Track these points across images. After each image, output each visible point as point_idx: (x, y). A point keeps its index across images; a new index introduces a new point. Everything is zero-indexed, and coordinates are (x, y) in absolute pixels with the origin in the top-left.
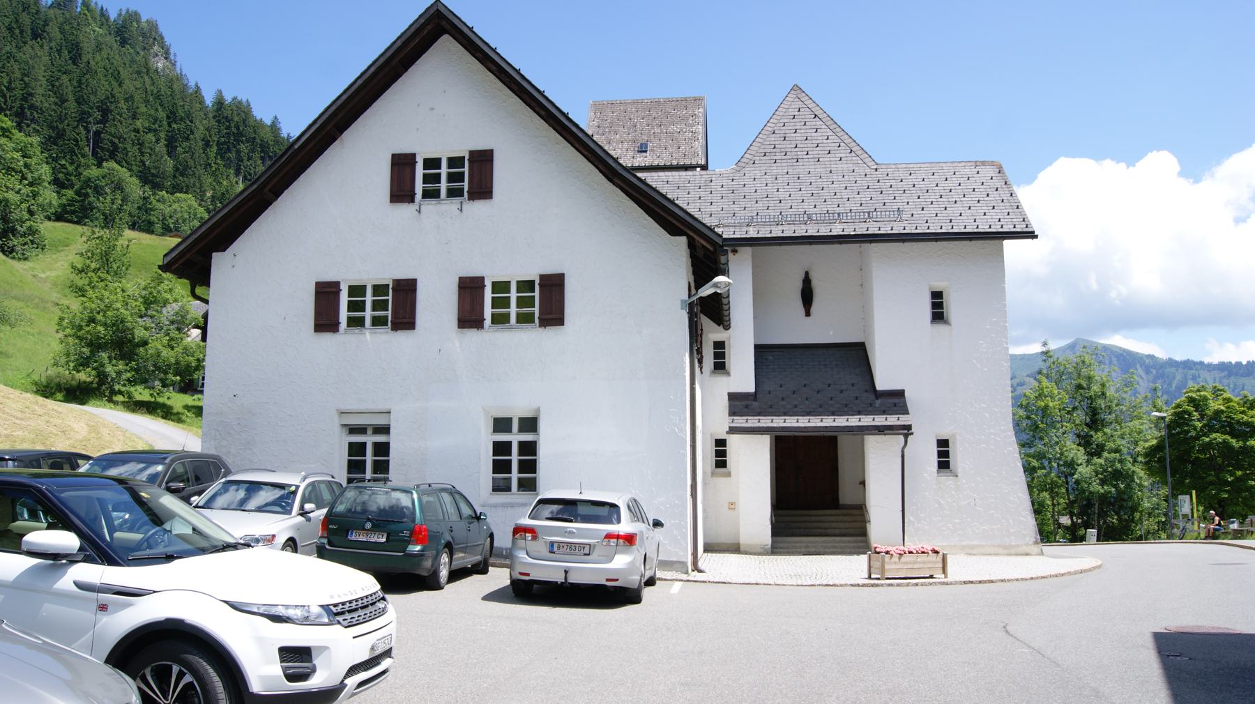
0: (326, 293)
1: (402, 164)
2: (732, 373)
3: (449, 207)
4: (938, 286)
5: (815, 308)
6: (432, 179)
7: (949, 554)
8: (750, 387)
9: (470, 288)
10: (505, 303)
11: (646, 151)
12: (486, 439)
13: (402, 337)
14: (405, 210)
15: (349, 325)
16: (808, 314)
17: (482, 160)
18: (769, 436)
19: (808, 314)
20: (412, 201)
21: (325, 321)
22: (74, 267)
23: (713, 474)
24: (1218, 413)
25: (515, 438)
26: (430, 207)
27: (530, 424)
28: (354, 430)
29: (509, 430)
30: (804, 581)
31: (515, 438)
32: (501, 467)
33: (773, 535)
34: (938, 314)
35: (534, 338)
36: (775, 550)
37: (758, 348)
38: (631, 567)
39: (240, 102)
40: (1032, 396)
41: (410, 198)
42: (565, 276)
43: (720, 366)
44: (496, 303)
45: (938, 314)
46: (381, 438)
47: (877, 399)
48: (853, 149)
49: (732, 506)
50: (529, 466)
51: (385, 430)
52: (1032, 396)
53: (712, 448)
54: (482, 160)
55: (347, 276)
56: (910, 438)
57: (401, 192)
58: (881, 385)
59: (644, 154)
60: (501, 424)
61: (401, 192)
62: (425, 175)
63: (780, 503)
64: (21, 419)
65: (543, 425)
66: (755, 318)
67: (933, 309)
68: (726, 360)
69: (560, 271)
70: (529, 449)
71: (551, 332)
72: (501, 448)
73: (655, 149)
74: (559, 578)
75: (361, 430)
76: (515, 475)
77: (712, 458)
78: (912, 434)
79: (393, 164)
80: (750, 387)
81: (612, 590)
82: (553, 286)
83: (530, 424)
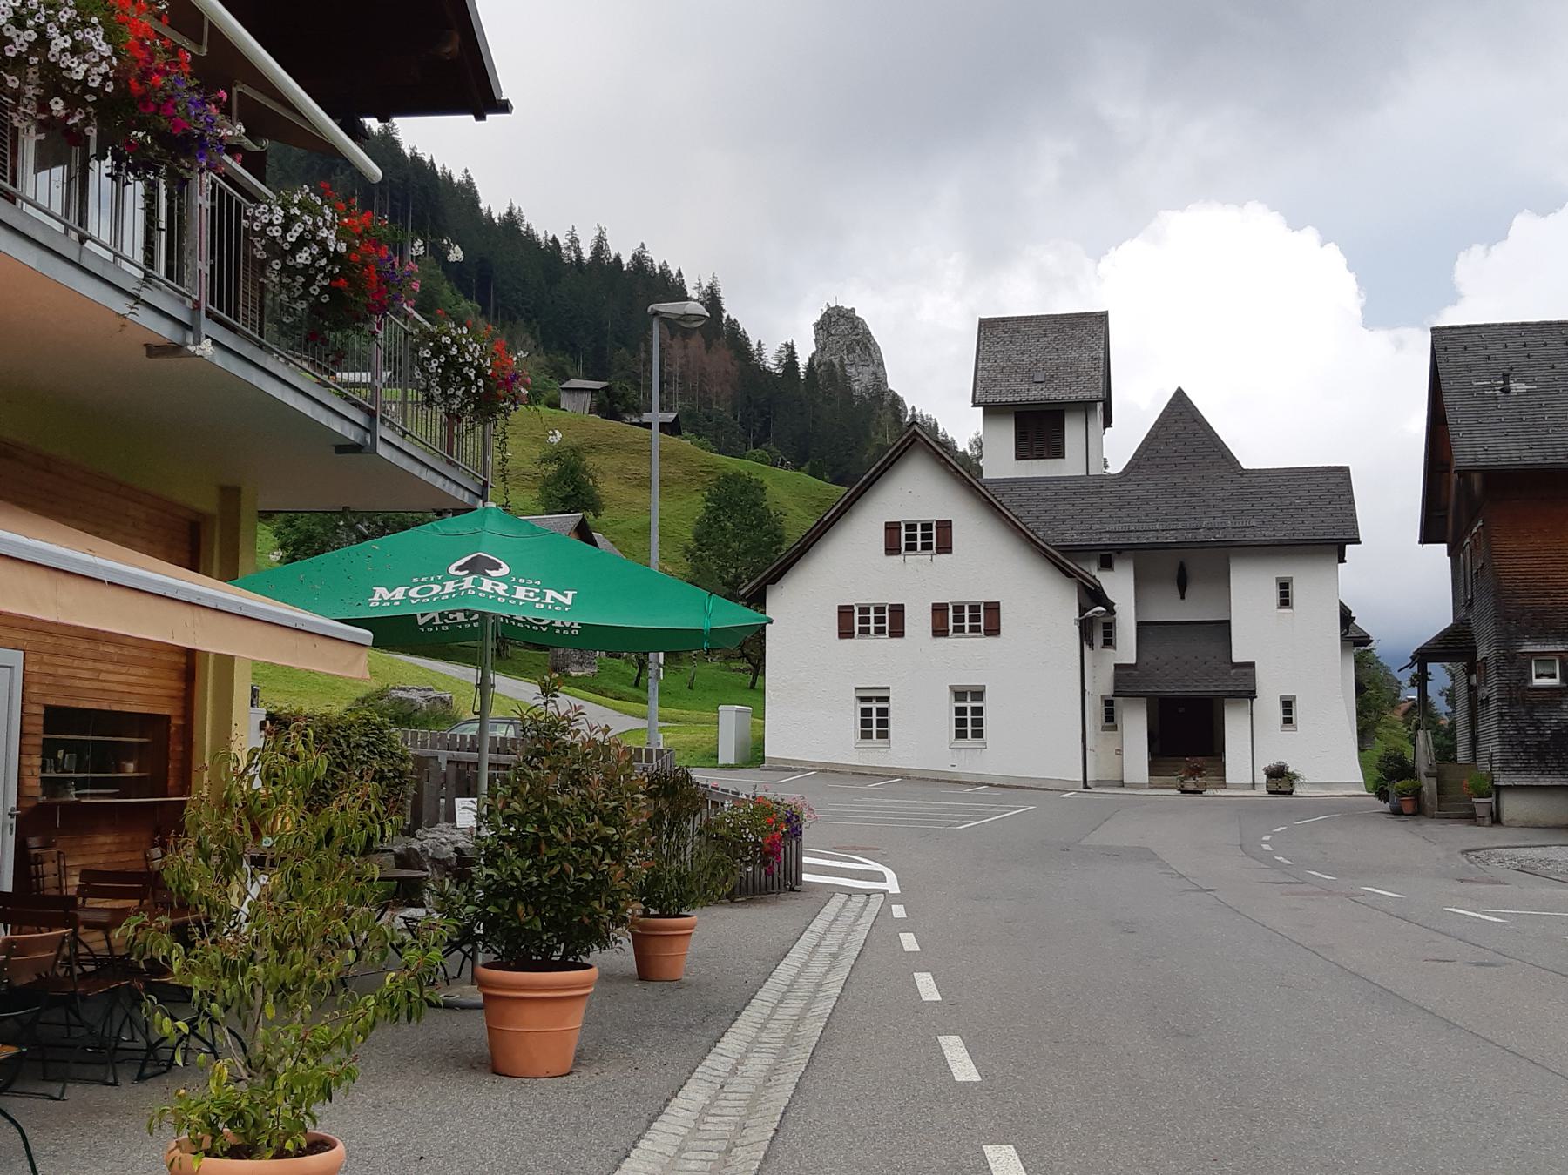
0: (845, 612)
1: (892, 529)
3: (925, 557)
7: (625, 978)
15: (860, 633)
16: (1183, 597)
17: (945, 526)
19: (1183, 597)
20: (900, 553)
21: (845, 632)
25: (969, 704)
26: (912, 558)
27: (979, 694)
28: (863, 699)
33: (1150, 775)
34: (1285, 602)
37: (1138, 624)
39: (421, 161)
40: (747, 1122)
41: (898, 552)
43: (1109, 642)
44: (956, 619)
45: (1285, 602)
47: (1233, 669)
51: (886, 699)
52: (747, 1122)
53: (1101, 707)
56: (1255, 700)
57: (892, 549)
60: (959, 694)
61: (892, 549)
65: (987, 696)
66: (1136, 602)
67: (1281, 596)
75: (869, 699)
76: (969, 728)
77: (1101, 715)
78: (1256, 697)
79: (886, 529)
83: (979, 694)
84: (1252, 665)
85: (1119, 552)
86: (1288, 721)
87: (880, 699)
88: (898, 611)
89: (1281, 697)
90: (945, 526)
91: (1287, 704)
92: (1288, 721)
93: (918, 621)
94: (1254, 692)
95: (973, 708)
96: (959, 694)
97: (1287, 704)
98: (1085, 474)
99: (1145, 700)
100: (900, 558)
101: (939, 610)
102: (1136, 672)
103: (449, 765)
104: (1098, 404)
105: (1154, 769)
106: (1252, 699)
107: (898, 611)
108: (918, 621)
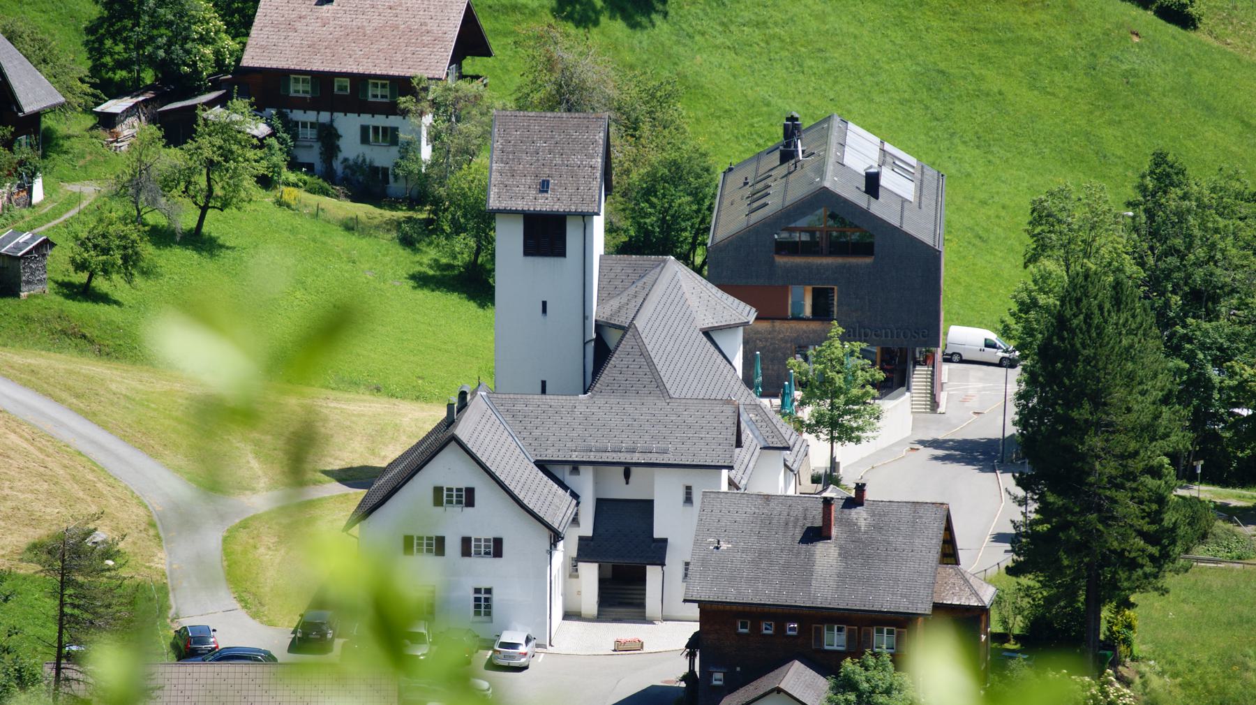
1: (438, 491)
2: (581, 523)
6: (450, 496)
8: (590, 533)
9: (466, 541)
11: (547, 192)
12: (472, 596)
14: (440, 509)
16: (627, 483)
17: (470, 492)
18: (596, 565)
19: (627, 483)
22: (73, 261)
24: (1027, 384)
25: (483, 596)
26: (450, 509)
27: (489, 591)
29: (480, 593)
30: (718, 361)
31: (483, 596)
32: (477, 606)
35: (491, 561)
36: (600, 617)
38: (526, 661)
42: (472, 306)
46: (487, 596)
49: (579, 593)
50: (488, 607)
54: (470, 492)
55: (416, 534)
58: (657, 535)
59: (546, 195)
60: (477, 591)
64: (77, 396)
70: (487, 600)
71: (497, 559)
72: (477, 600)
73: (556, 187)
74: (507, 664)
80: (590, 533)
82: (498, 542)
83: (489, 591)
95: (485, 598)
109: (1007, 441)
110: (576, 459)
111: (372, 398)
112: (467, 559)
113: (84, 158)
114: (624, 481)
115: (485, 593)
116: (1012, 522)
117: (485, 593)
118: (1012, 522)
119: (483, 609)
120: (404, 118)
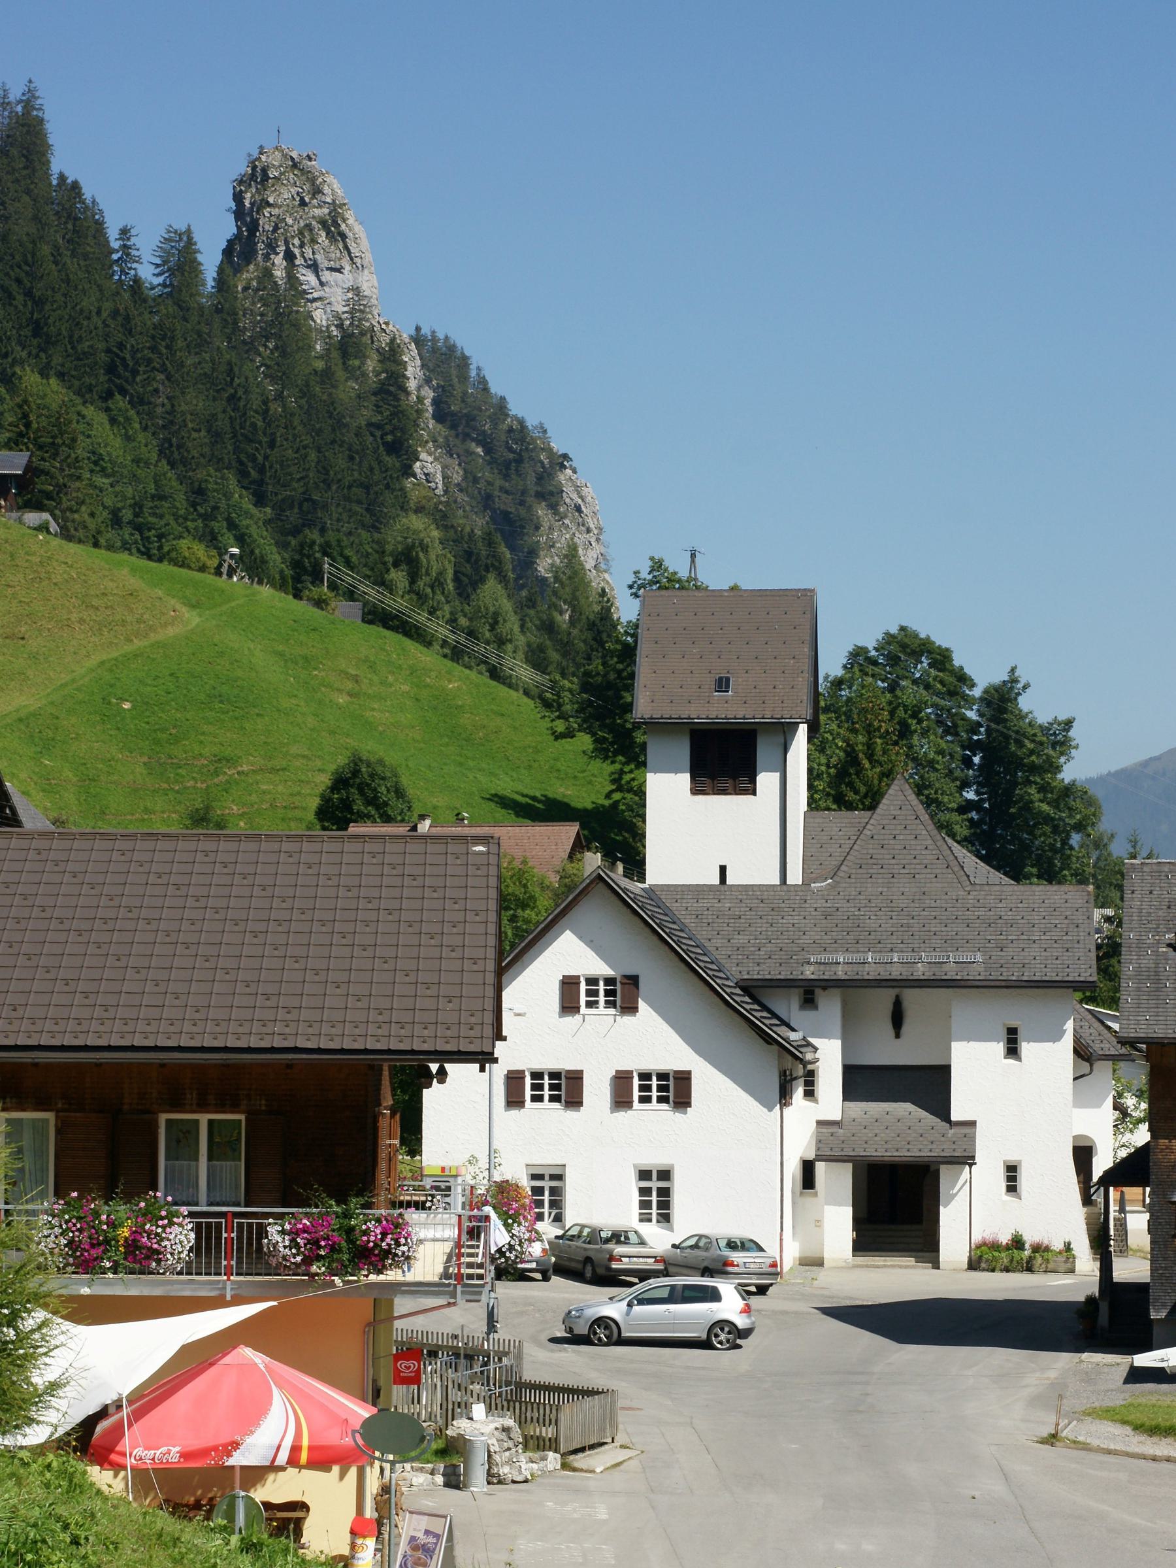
4: (1013, 1024)
5: (905, 1029)
9: (621, 1081)
10: (648, 1088)
13: (571, 1114)
16: (898, 1036)
17: (684, 1078)
19: (898, 1036)
23: (801, 1194)
25: (654, 1184)
27: (665, 1175)
29: (650, 1179)
32: (645, 1205)
46: (554, 1184)
48: (951, 864)
50: (665, 1205)
60: (644, 1175)
62: (587, 1001)
63: (860, 1223)
68: (815, 1079)
69: (635, 974)
70: (554, 1191)
72: (644, 1192)
81: (1082, 1176)
83: (665, 1175)
84: (972, 1124)
85: (824, 988)
86: (1012, 1189)
87: (554, 1177)
88: (576, 1078)
89: (1004, 1162)
90: (684, 1078)
91: (1012, 1172)
92: (1012, 1189)
93: (597, 1091)
94: (973, 1158)
95: (658, 1189)
96: (644, 1175)
97: (1012, 1172)
98: (776, 881)
99: (850, 1165)
100: (578, 1018)
101: (621, 1081)
102: (841, 1131)
103: (1036, 1268)
104: (801, 725)
105: (861, 1246)
106: (971, 1165)
107: (576, 1078)
108: (597, 1091)
109: (341, 1469)
110: (813, 977)
111: (533, 824)
112: (622, 1115)
113: (23, 348)
114: (891, 1032)
115: (659, 1179)
116: (189, 226)
117: (659, 1179)
118: (189, 226)
119: (546, 1210)
120: (1069, 724)
